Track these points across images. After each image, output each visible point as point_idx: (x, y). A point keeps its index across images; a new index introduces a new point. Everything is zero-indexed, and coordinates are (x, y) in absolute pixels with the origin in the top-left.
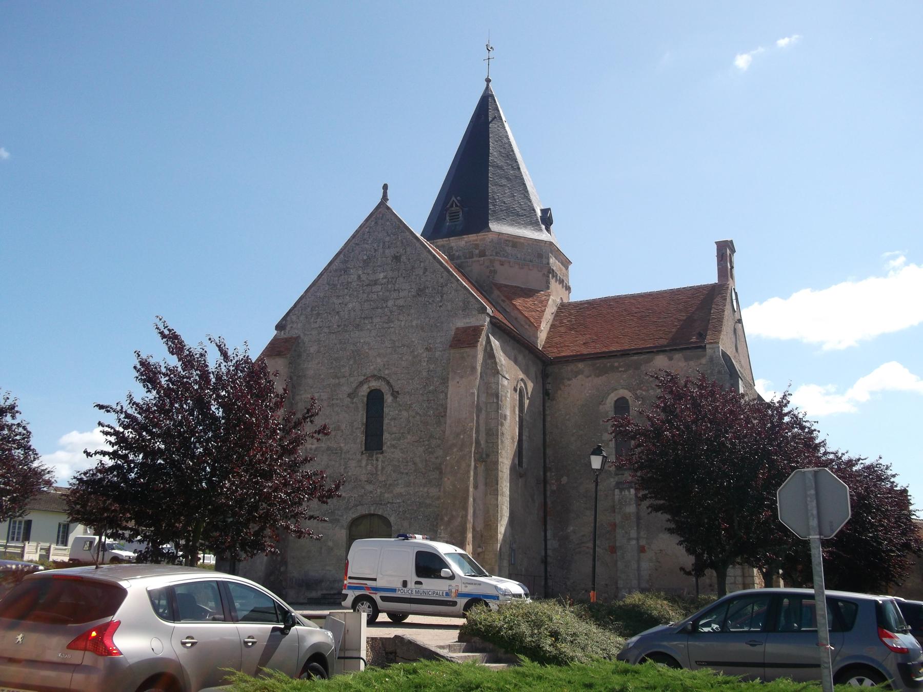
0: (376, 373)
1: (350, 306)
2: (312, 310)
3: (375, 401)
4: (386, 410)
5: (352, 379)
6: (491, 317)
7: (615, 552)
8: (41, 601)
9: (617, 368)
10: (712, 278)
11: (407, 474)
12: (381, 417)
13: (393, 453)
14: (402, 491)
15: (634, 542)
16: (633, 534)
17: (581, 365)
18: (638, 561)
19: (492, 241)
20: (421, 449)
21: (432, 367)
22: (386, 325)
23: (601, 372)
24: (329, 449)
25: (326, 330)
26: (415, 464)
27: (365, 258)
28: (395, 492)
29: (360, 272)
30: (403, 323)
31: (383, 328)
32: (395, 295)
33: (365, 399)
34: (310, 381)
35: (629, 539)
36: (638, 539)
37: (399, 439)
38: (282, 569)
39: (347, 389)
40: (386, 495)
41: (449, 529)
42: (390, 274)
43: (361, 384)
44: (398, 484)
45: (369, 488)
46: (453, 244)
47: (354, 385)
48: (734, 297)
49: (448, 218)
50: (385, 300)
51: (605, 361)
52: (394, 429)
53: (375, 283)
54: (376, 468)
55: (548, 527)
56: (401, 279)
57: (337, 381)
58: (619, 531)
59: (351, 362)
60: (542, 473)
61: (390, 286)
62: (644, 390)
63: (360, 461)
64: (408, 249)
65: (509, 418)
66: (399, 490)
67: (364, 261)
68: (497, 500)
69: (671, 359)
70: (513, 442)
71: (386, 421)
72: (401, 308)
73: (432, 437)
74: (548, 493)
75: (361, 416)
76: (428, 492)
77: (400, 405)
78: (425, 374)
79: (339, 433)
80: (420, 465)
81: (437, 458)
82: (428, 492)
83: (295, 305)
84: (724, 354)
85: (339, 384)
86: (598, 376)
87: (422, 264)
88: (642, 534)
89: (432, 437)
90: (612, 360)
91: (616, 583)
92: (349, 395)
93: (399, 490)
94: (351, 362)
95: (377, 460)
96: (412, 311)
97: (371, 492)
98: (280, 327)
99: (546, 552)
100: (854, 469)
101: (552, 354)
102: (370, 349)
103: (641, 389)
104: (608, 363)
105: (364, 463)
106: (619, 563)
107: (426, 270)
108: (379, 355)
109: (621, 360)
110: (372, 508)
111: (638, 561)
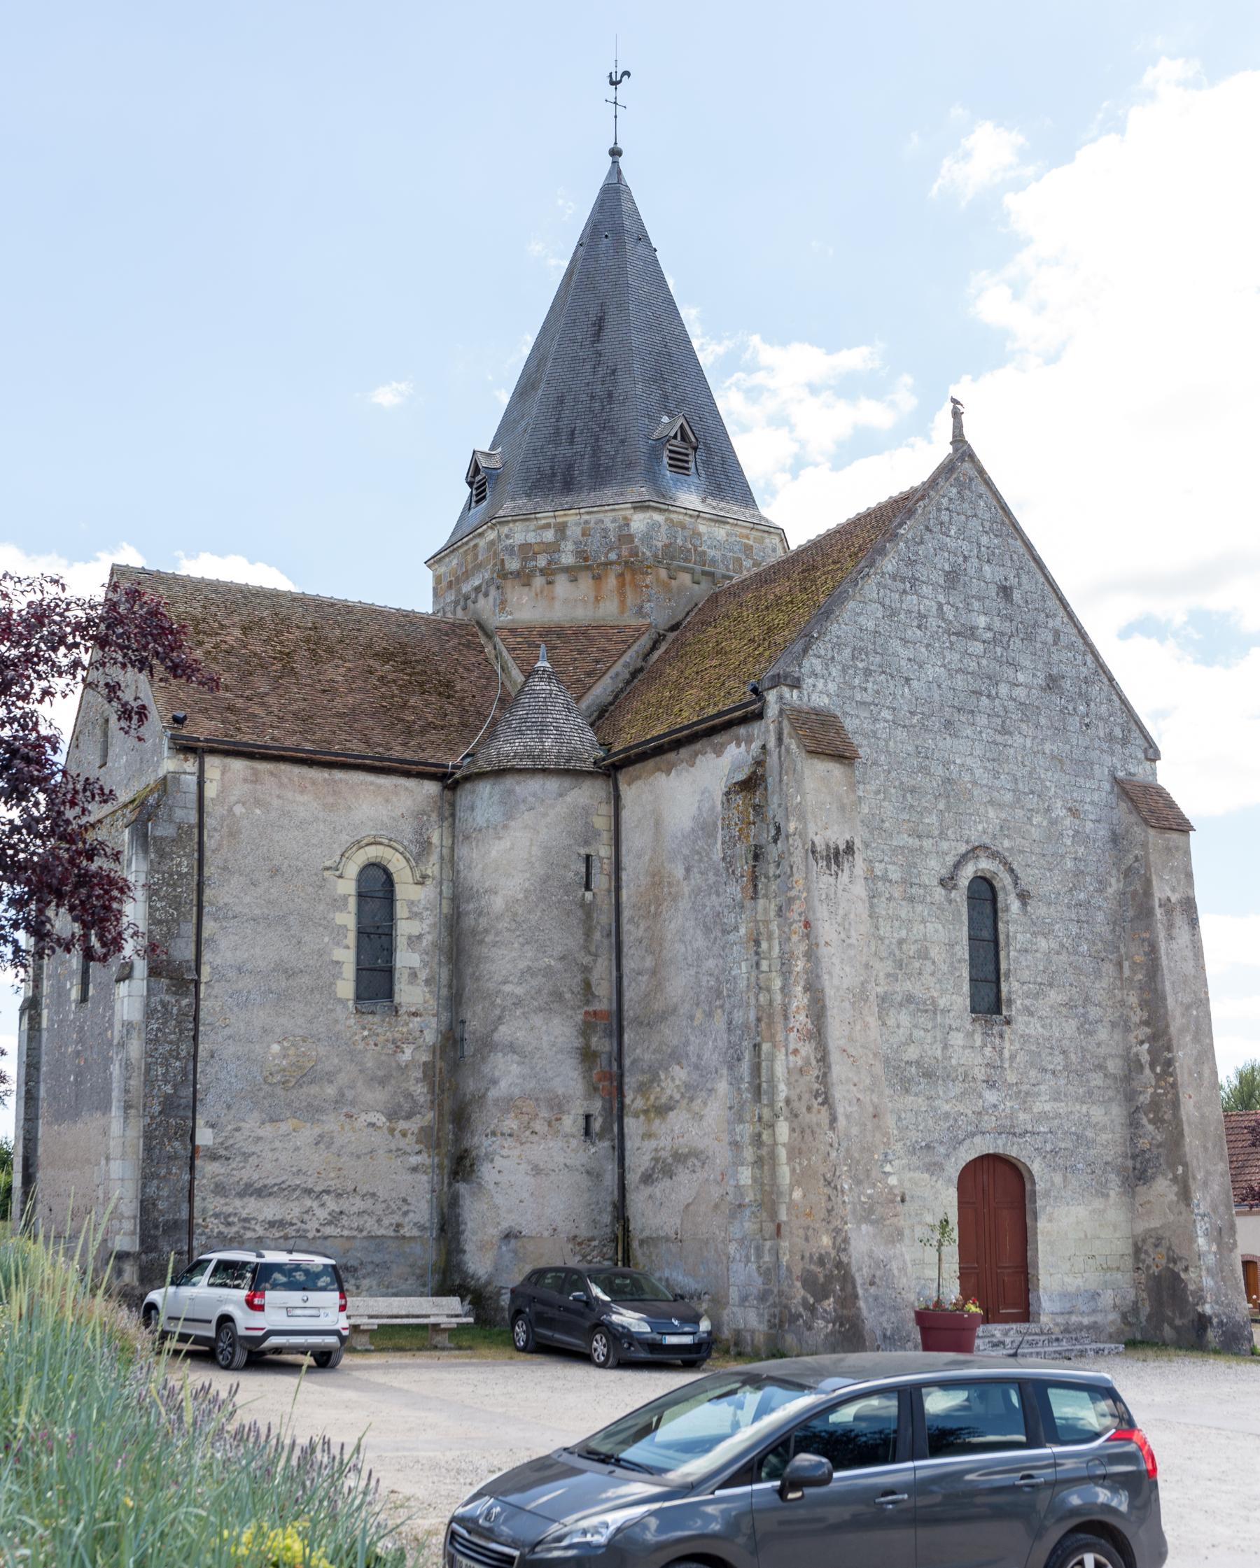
3: (984, 896)
5: (945, 845)
8: (56, 1429)
13: (1027, 1024)
14: (1048, 1107)
22: (999, 739)
24: (909, 999)
29: (941, 598)
37: (1036, 996)
45: (991, 1097)
47: (950, 860)
54: (1001, 1054)
66: (1043, 1105)
76: (1088, 1115)
81: (1099, 1045)
82: (1088, 1115)
93: (1043, 1105)
94: (941, 806)
110: (1000, 1142)
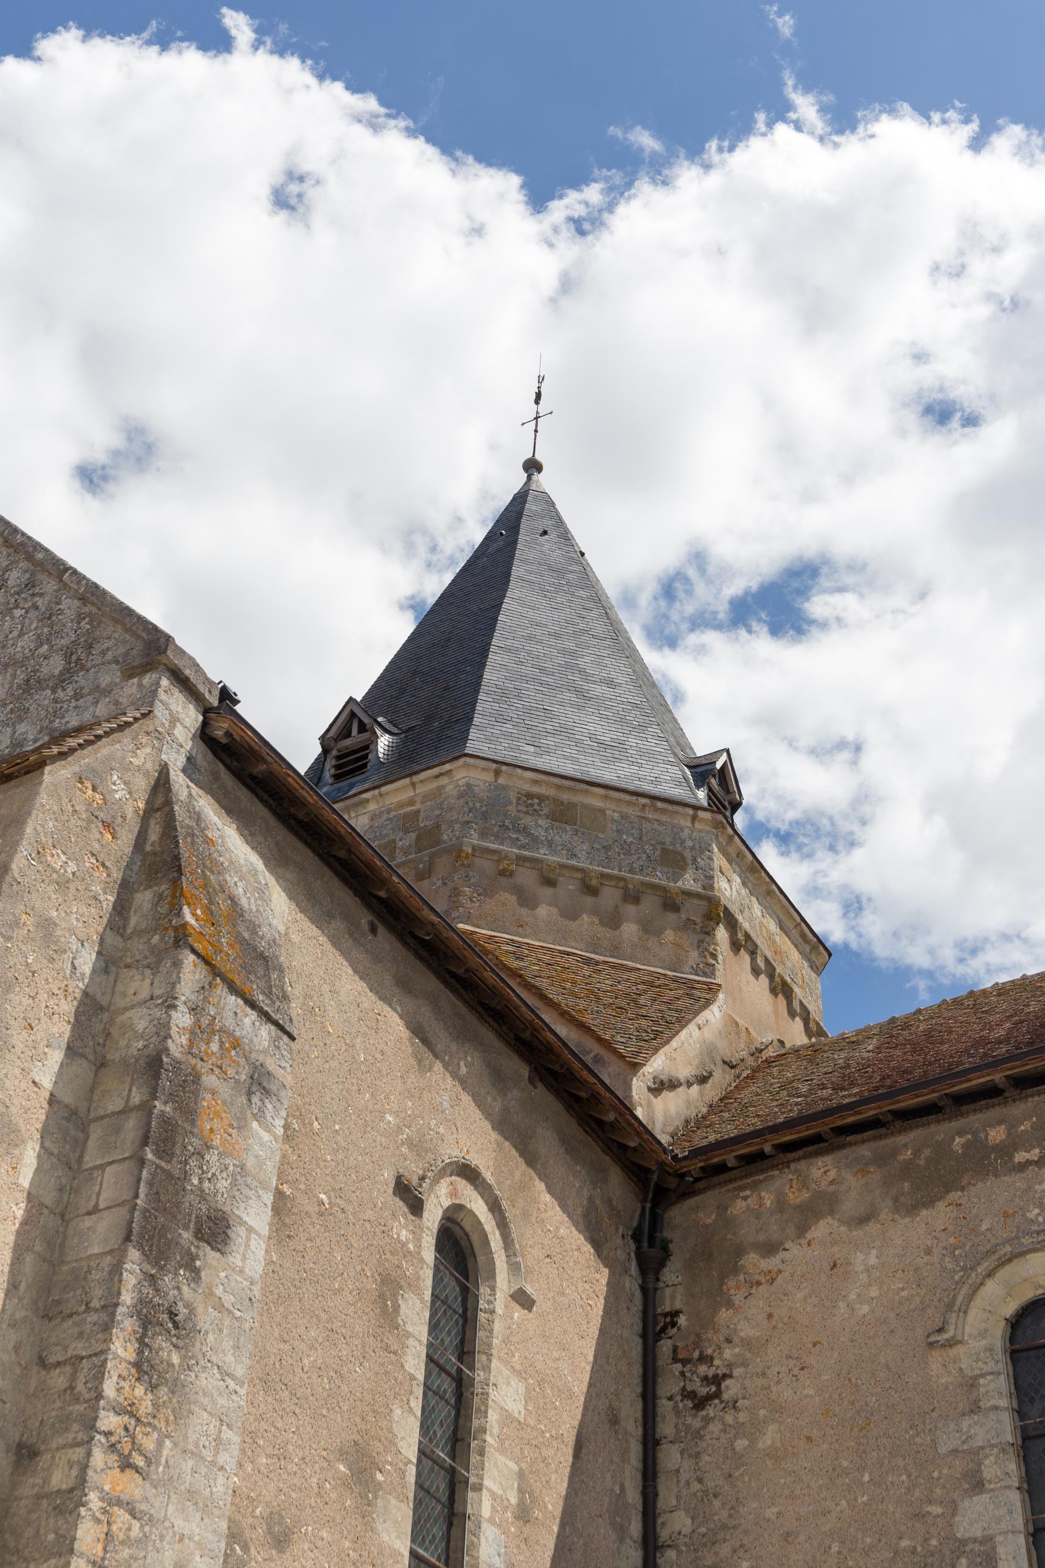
9: (1005, 1150)
17: (822, 1170)
19: (467, 792)
23: (929, 1185)
51: (939, 1130)
86: (913, 1209)
90: (974, 1119)
100: (255, 1125)
104: (953, 1134)
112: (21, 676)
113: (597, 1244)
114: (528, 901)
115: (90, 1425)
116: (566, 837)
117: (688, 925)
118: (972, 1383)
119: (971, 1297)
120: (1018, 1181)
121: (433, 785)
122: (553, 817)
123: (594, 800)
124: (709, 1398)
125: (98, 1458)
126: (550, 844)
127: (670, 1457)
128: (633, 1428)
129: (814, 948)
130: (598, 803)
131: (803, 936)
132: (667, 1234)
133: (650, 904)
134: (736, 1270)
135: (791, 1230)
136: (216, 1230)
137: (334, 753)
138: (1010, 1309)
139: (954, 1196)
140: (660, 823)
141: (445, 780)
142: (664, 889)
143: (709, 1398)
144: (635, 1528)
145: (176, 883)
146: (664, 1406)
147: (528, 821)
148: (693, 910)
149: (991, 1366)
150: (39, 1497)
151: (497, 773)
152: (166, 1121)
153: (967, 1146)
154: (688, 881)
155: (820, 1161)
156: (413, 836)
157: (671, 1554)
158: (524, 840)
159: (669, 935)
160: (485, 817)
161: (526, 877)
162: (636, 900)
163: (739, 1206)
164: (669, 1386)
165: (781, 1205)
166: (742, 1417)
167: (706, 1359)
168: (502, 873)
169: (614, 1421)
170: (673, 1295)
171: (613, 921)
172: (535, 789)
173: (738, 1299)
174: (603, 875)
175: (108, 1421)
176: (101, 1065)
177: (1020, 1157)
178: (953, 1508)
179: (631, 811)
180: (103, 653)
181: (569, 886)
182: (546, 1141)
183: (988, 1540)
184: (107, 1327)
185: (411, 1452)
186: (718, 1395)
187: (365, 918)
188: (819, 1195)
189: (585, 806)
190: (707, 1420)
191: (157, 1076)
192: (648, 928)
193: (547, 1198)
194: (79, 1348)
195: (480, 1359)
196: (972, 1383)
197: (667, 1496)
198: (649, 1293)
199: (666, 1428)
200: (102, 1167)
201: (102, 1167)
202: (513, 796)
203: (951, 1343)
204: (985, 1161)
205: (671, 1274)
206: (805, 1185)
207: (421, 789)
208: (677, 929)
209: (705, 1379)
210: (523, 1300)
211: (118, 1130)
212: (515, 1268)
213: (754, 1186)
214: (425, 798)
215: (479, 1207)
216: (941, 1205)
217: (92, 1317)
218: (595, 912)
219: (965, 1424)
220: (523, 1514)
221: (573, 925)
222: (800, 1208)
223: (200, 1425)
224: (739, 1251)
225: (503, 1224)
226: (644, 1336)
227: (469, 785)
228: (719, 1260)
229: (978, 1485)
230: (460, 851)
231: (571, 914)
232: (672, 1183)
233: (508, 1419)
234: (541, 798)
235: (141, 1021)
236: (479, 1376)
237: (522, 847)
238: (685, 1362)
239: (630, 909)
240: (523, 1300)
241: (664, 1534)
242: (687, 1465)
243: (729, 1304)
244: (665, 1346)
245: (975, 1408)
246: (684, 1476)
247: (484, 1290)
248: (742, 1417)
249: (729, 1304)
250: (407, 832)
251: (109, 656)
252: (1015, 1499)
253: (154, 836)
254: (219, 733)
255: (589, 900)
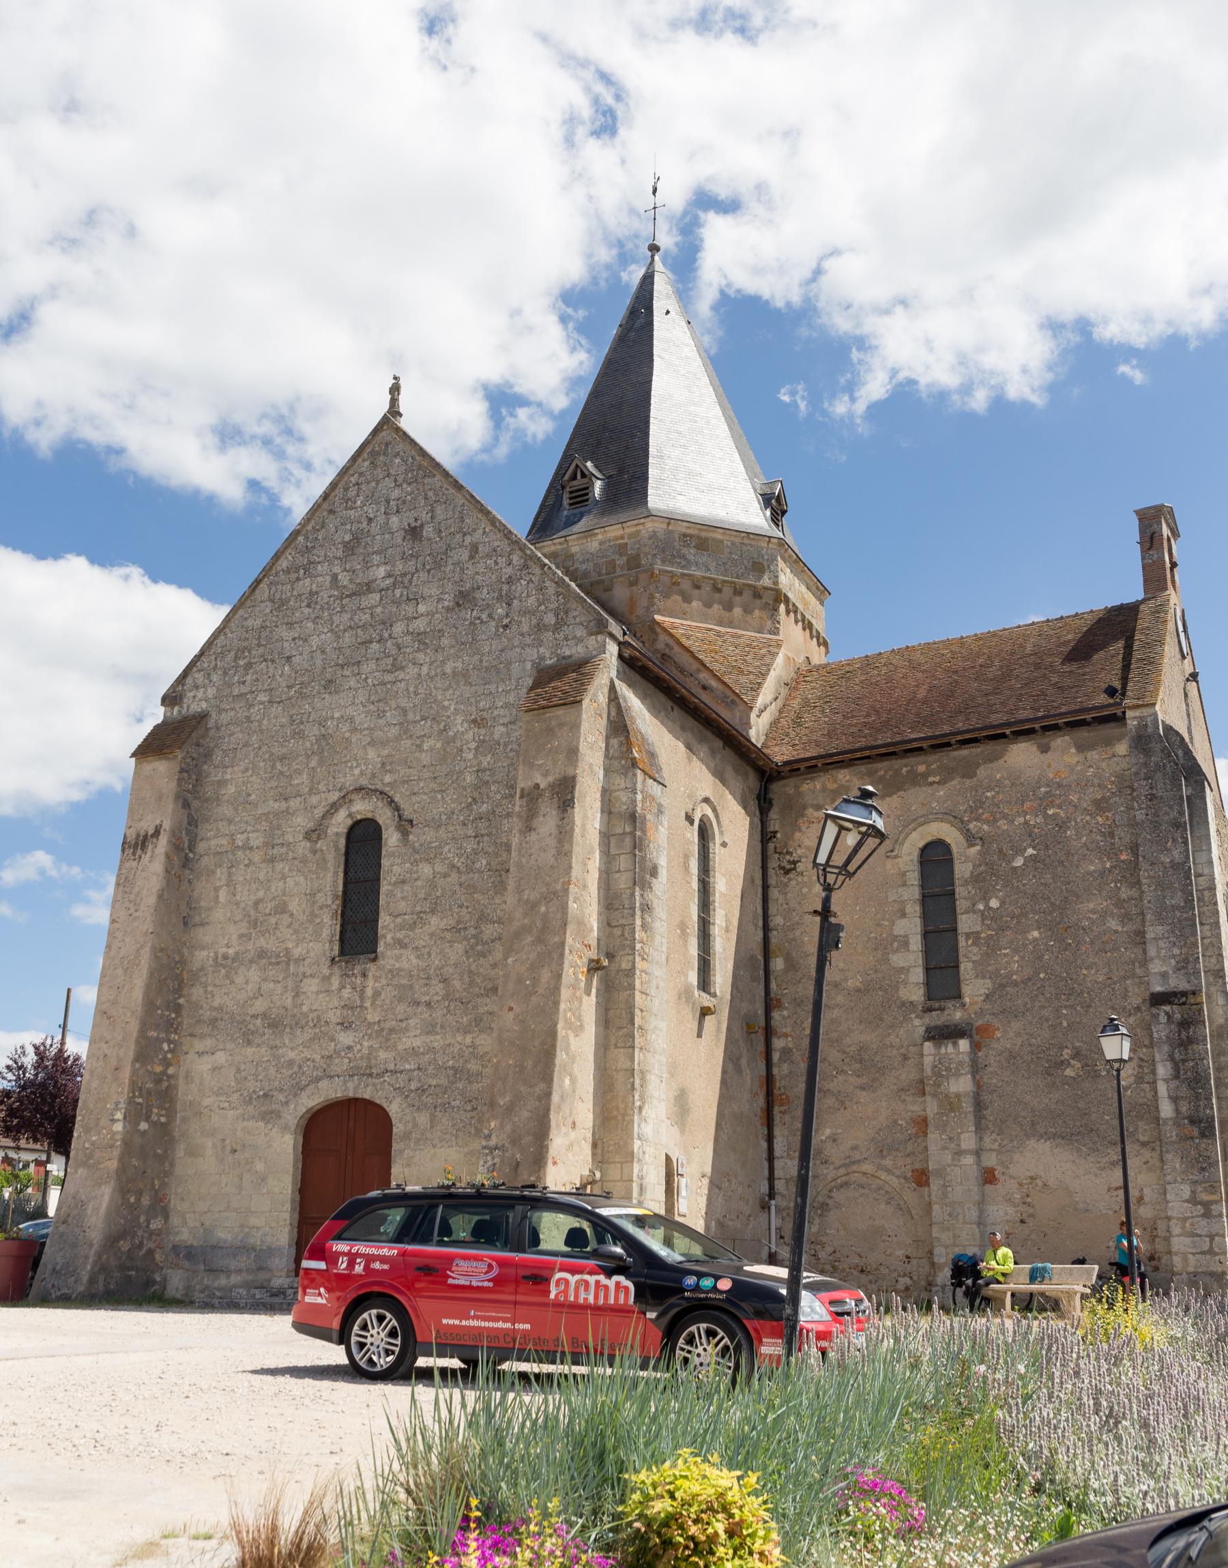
0: (364, 782)
1: (315, 642)
2: (236, 658)
3: (363, 842)
4: (385, 862)
5: (314, 800)
6: (619, 644)
7: (927, 1184)
9: (925, 776)
10: (1132, 591)
11: (428, 1004)
12: (374, 882)
13: (398, 958)
14: (417, 1042)
15: (969, 1160)
16: (968, 1141)
18: (981, 1203)
19: (653, 535)
20: (459, 948)
21: (486, 761)
22: (389, 677)
24: (262, 954)
25: (263, 697)
26: (444, 980)
27: (347, 538)
28: (400, 1047)
29: (337, 569)
30: (425, 669)
31: (383, 684)
32: (409, 609)
33: (343, 842)
34: (227, 811)
35: (959, 1153)
36: (978, 1153)
37: (413, 926)
38: (156, 1224)
39: (302, 822)
40: (383, 1055)
41: (508, 1128)
42: (400, 566)
43: (334, 807)
44: (407, 1030)
45: (346, 1038)
46: (575, 549)
47: (319, 812)
48: (1181, 628)
49: (566, 502)
50: (387, 623)
51: (896, 763)
52: (402, 906)
53: (368, 587)
55: (777, 1132)
56: (423, 576)
57: (284, 805)
58: (934, 1137)
59: (313, 763)
60: (761, 1012)
61: (398, 592)
62: (987, 822)
63: (327, 979)
64: (439, 510)
65: (663, 874)
66: (412, 1040)
67: (346, 545)
68: (632, 1059)
69: (1045, 749)
70: (684, 934)
71: (384, 888)
72: (419, 637)
73: (482, 918)
74: (776, 1057)
75: (331, 881)
76: (473, 1046)
77: (415, 851)
78: (469, 778)
79: (286, 919)
80: (457, 984)
83: (202, 653)
84: (1169, 729)
85: (287, 811)
87: (468, 539)
88: (987, 1141)
89: (482, 918)
90: (912, 760)
91: (931, 1253)
92: (308, 835)
94: (313, 763)
95: (364, 975)
96: (445, 642)
97: (349, 1048)
98: (170, 699)
99: (771, 1187)
101: (780, 754)
102: (354, 730)
103: (977, 819)
104: (903, 766)
105: (335, 983)
106: (936, 1208)
107: (474, 549)
108: (372, 743)
109: (931, 758)
110: (350, 1085)
111: (981, 1203)
112: (534, 622)
113: (745, 808)
114: (687, 599)
115: (634, 948)
116: (704, 559)
117: (765, 607)
118: (904, 874)
119: (905, 839)
120: (929, 790)
121: (634, 529)
122: (698, 547)
123: (718, 535)
124: (791, 870)
125: (638, 959)
126: (697, 564)
127: (774, 893)
128: (759, 882)
129: (822, 592)
130: (720, 537)
131: (818, 588)
132: (771, 796)
133: (747, 594)
134: (803, 815)
135: (828, 800)
136: (654, 872)
137: (568, 489)
138: (921, 844)
139: (901, 793)
140: (752, 546)
141: (641, 527)
142: (755, 587)
143: (791, 870)
144: (760, 923)
145: (627, 737)
146: (771, 872)
147: (685, 551)
148: (768, 598)
149: (912, 868)
150: (618, 971)
151: (668, 524)
152: (640, 838)
153: (908, 772)
154: (766, 581)
155: (842, 771)
156: (625, 558)
157: (775, 933)
158: (684, 563)
159: (757, 613)
160: (663, 551)
161: (686, 585)
162: (740, 594)
163: (805, 787)
164: (773, 863)
165: (824, 789)
166: (805, 879)
167: (790, 854)
168: (674, 584)
169: (753, 882)
170: (774, 825)
171: (729, 607)
172: (688, 531)
173: (803, 828)
174: (724, 581)
175: (638, 946)
176: (610, 813)
177: (931, 779)
178: (893, 923)
179: (736, 540)
180: (575, 617)
181: (707, 588)
182: (729, 773)
183: (906, 936)
184: (633, 915)
185: (695, 918)
186: (795, 869)
187: (670, 704)
188: (841, 786)
189: (713, 539)
190: (790, 879)
191: (635, 821)
192: (747, 610)
193: (730, 797)
194: (623, 921)
195: (711, 873)
196: (904, 874)
197: (773, 910)
198: (763, 823)
199: (772, 881)
200: (619, 855)
201: (619, 855)
202: (677, 536)
203: (896, 857)
204: (916, 779)
205: (774, 814)
206: (835, 781)
207: (628, 531)
208: (761, 609)
209: (789, 861)
210: (724, 845)
211: (623, 841)
212: (721, 833)
213: (811, 779)
214: (630, 536)
215: (709, 812)
216: (895, 797)
217: (626, 911)
218: (720, 603)
219: (900, 890)
220: (727, 930)
221: (710, 611)
222: (832, 791)
223: (658, 939)
224: (805, 807)
225: (717, 816)
226: (762, 841)
227: (654, 532)
228: (795, 810)
229: (904, 915)
230: (653, 573)
231: (708, 605)
232: (775, 774)
233: (722, 894)
234: (691, 536)
235: (624, 797)
236: (712, 880)
237: (682, 568)
238: (780, 853)
239: (737, 599)
240: (724, 845)
241: (771, 925)
242: (781, 897)
243: (800, 830)
244: (771, 846)
245: (904, 884)
246: (780, 901)
247: (711, 845)
248: (805, 879)
249: (800, 830)
250: (621, 555)
251: (578, 620)
252: (918, 921)
253: (613, 714)
254: (626, 655)
255: (717, 595)
